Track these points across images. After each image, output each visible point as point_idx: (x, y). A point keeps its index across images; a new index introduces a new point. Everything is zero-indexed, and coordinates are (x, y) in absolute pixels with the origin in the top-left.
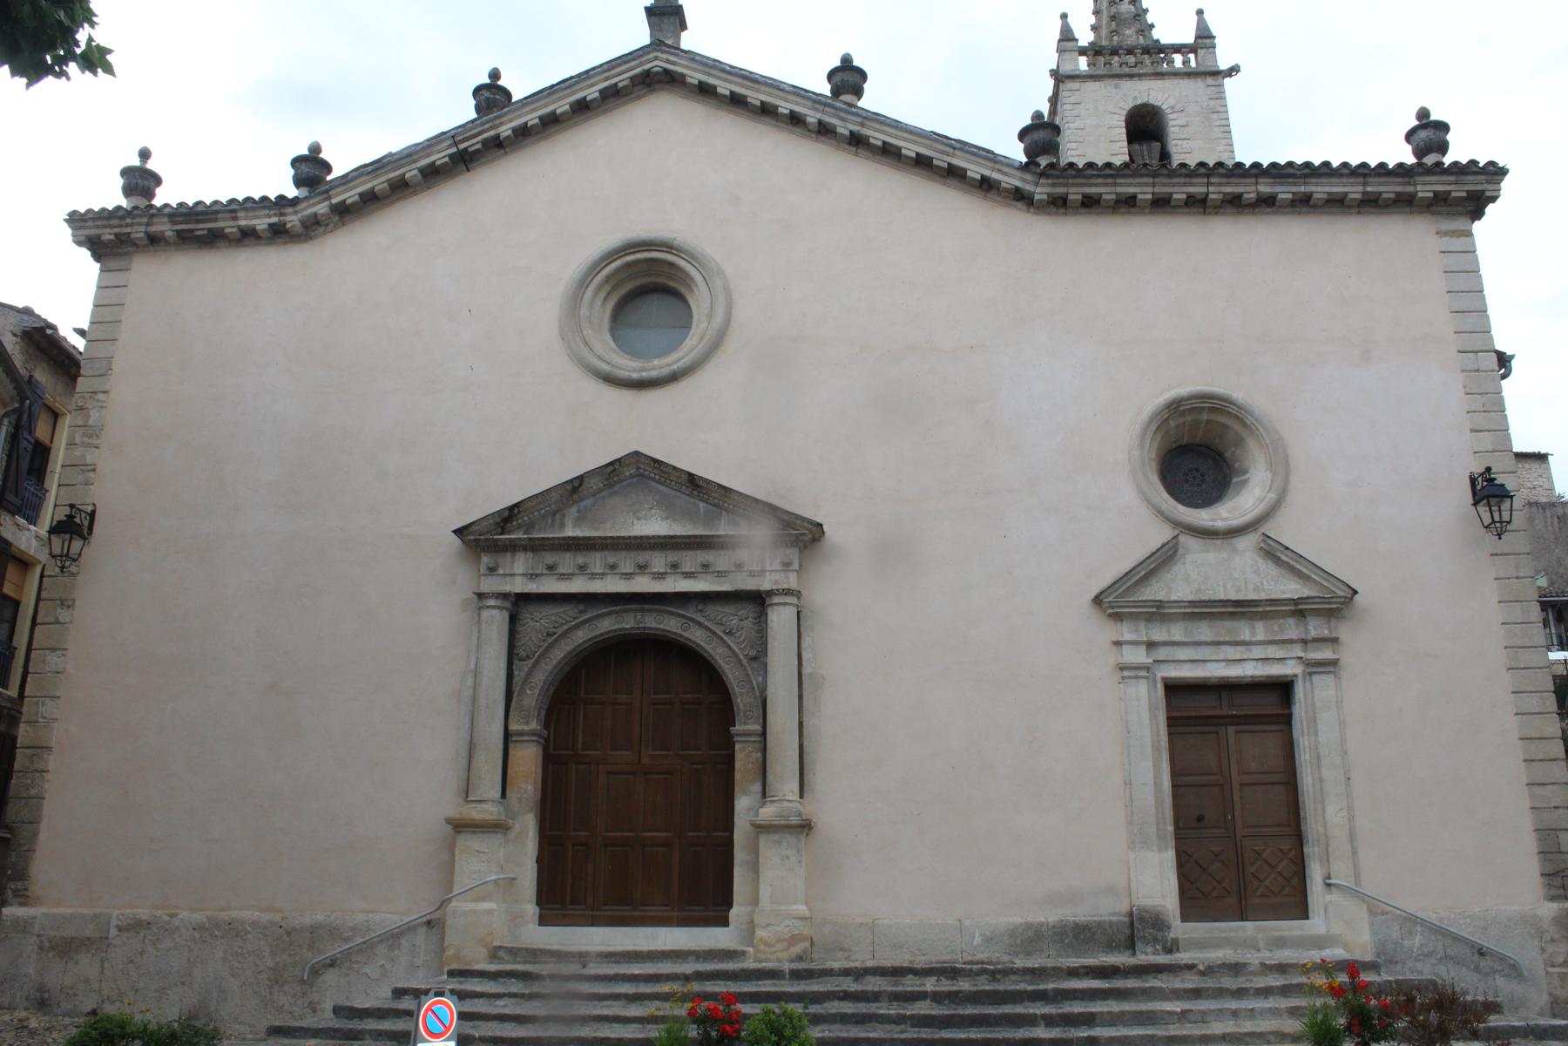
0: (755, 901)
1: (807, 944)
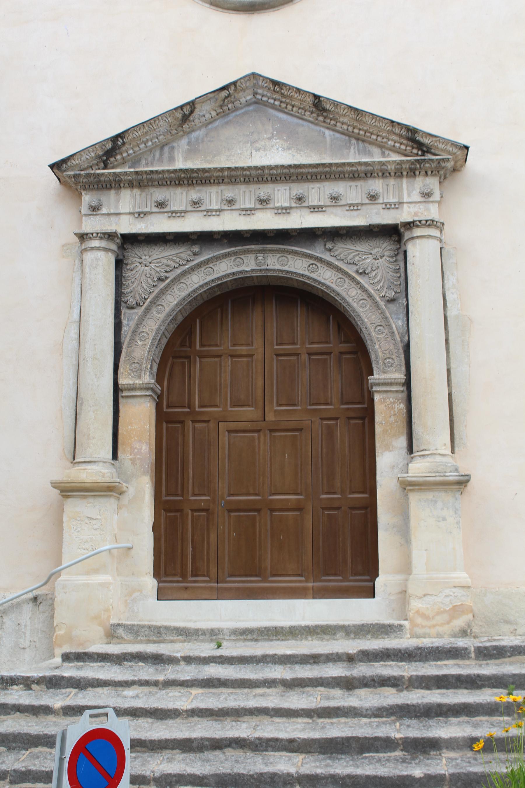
0: (406, 568)
1: (470, 616)
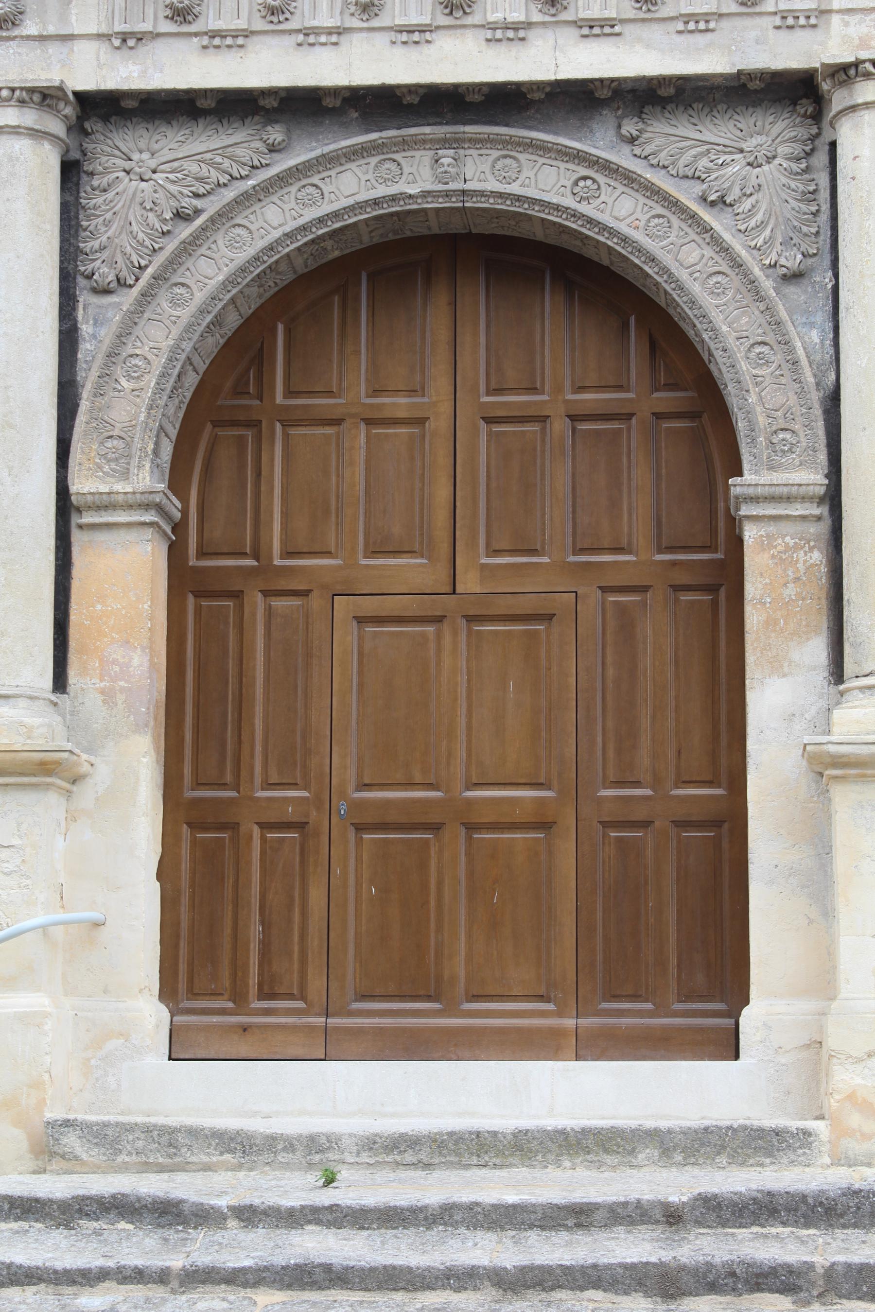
0: (823, 982)
